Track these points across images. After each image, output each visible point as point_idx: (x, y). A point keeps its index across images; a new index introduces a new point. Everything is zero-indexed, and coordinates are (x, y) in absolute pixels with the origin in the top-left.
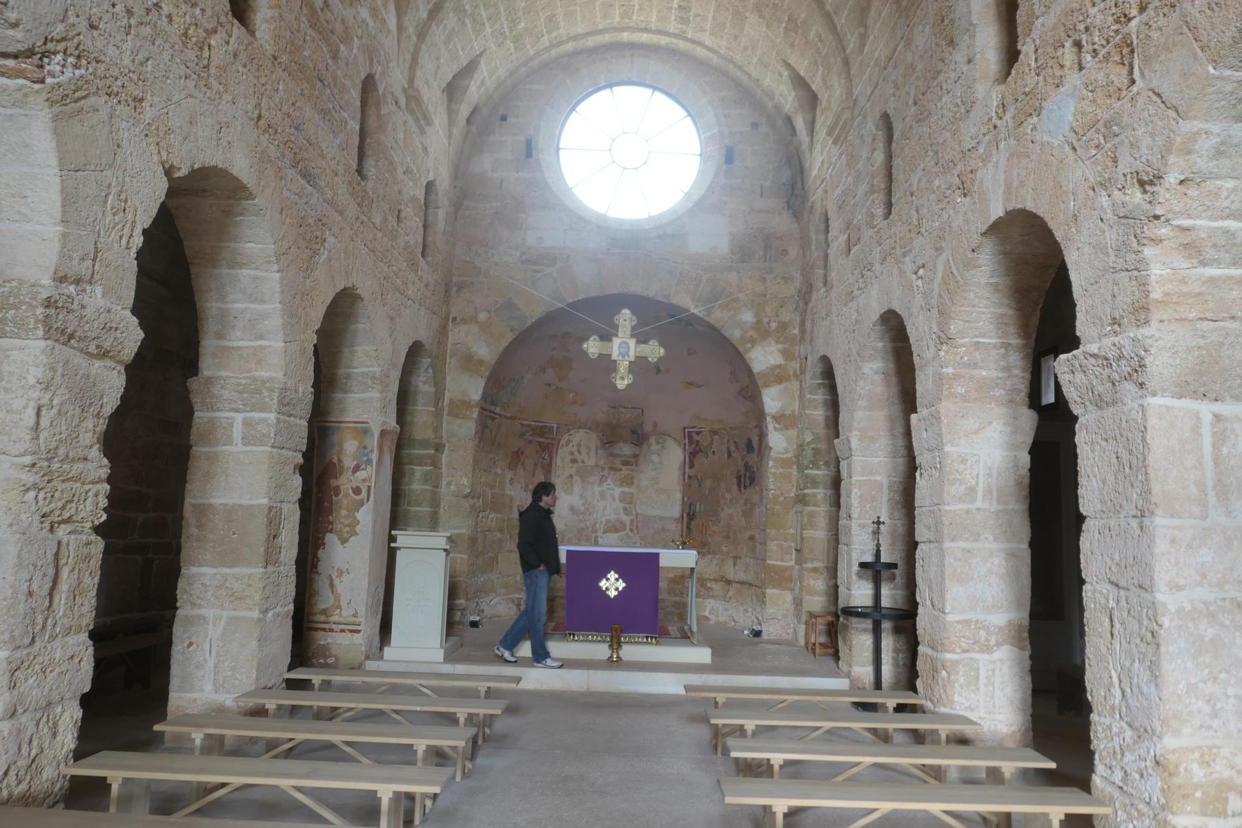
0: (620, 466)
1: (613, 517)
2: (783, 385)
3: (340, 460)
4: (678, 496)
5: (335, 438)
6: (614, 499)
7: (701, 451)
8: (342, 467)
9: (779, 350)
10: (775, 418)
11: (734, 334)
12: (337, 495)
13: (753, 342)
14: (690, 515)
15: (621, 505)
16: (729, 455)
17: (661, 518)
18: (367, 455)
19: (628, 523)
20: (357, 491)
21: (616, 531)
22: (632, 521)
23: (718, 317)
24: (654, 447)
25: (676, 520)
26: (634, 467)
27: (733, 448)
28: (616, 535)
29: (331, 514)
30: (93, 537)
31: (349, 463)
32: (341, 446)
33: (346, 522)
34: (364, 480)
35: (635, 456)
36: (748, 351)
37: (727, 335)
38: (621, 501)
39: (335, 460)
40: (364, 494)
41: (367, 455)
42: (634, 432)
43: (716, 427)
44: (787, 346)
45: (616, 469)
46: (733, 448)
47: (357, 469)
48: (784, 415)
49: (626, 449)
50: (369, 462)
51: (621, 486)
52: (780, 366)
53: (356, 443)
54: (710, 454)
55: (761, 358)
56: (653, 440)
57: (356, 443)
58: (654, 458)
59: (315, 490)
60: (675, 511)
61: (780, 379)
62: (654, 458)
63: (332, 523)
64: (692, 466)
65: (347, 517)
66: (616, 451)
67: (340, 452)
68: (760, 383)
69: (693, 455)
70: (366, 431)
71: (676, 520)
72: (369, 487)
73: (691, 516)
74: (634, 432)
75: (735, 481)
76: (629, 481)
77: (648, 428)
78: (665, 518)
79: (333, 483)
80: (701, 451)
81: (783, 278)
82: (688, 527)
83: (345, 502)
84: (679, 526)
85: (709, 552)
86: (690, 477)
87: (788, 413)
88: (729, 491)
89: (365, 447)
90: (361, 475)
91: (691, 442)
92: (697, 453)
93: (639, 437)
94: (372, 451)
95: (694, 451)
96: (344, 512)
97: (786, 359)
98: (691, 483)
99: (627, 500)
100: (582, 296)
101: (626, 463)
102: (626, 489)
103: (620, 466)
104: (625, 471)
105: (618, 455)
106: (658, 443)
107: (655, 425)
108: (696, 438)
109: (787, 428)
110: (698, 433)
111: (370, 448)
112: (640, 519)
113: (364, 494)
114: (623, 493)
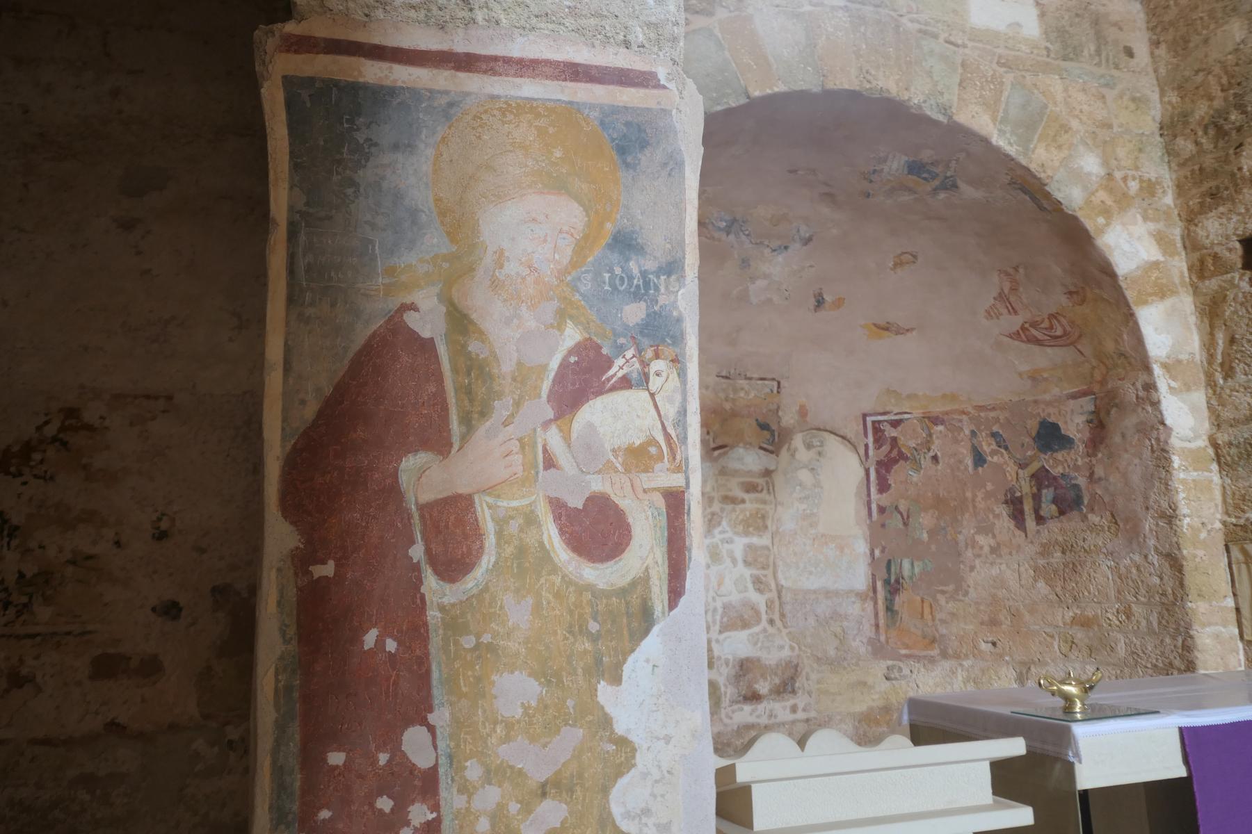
0: (740, 494)
1: (735, 598)
2: (1169, 302)
3: (460, 322)
4: (862, 547)
5: (415, 173)
6: (734, 561)
7: (902, 456)
8: (477, 371)
9: (1150, 234)
10: (1165, 366)
11: (1071, 196)
12: (453, 566)
13: (1107, 212)
14: (889, 584)
15: (747, 573)
16: (979, 459)
17: (828, 594)
18: (643, 290)
19: (763, 608)
20: (598, 530)
21: (745, 625)
22: (769, 605)
23: (1040, 158)
24: (803, 455)
25: (862, 596)
26: (764, 495)
27: (987, 446)
28: (746, 632)
29: (419, 712)
30: (1238, 245)
31: (524, 336)
32: (460, 227)
33: (537, 763)
34: (639, 457)
35: (767, 473)
36: (1102, 231)
37: (1059, 196)
38: (747, 563)
39: (427, 321)
40: (645, 550)
41: (643, 290)
42: (764, 427)
43: (937, 409)
44: (1161, 226)
45: (733, 500)
46: (987, 446)
47: (583, 379)
48: (1179, 362)
49: (749, 460)
50: (658, 333)
51: (747, 534)
52: (1156, 264)
53: (568, 215)
54: (926, 462)
55: (1126, 247)
56: (798, 441)
57: (568, 215)
58: (804, 476)
59: (280, 537)
60: (859, 577)
61: (1163, 292)
62: (804, 476)
63: (428, 784)
64: (883, 487)
65: (541, 722)
66: (734, 465)
67: (460, 265)
68: (1130, 295)
69: (885, 466)
70: (632, 140)
71: (862, 596)
72: (675, 501)
73: (894, 587)
74: (764, 427)
75: (1003, 510)
76: (757, 523)
77: (789, 418)
78: (837, 593)
79: (420, 477)
80: (902, 456)
81: (1134, 99)
82: (889, 609)
83: (517, 614)
84: (869, 606)
85: (944, 655)
86: (882, 510)
87: (1184, 357)
88: (987, 530)
89: (625, 243)
90: (614, 418)
91: (879, 441)
92: (896, 461)
93: (772, 437)
94: (672, 268)
95: (887, 454)
96: (515, 691)
97: (1165, 253)
98: (885, 521)
99: (754, 558)
100: (780, 88)
101: (751, 488)
102: (755, 540)
103: (740, 494)
104: (751, 504)
105: (735, 473)
106: (809, 446)
107: (803, 412)
108: (890, 432)
109: (1188, 389)
110: (895, 424)
111: (656, 241)
112: (787, 597)
113: (645, 550)
114: (750, 548)
